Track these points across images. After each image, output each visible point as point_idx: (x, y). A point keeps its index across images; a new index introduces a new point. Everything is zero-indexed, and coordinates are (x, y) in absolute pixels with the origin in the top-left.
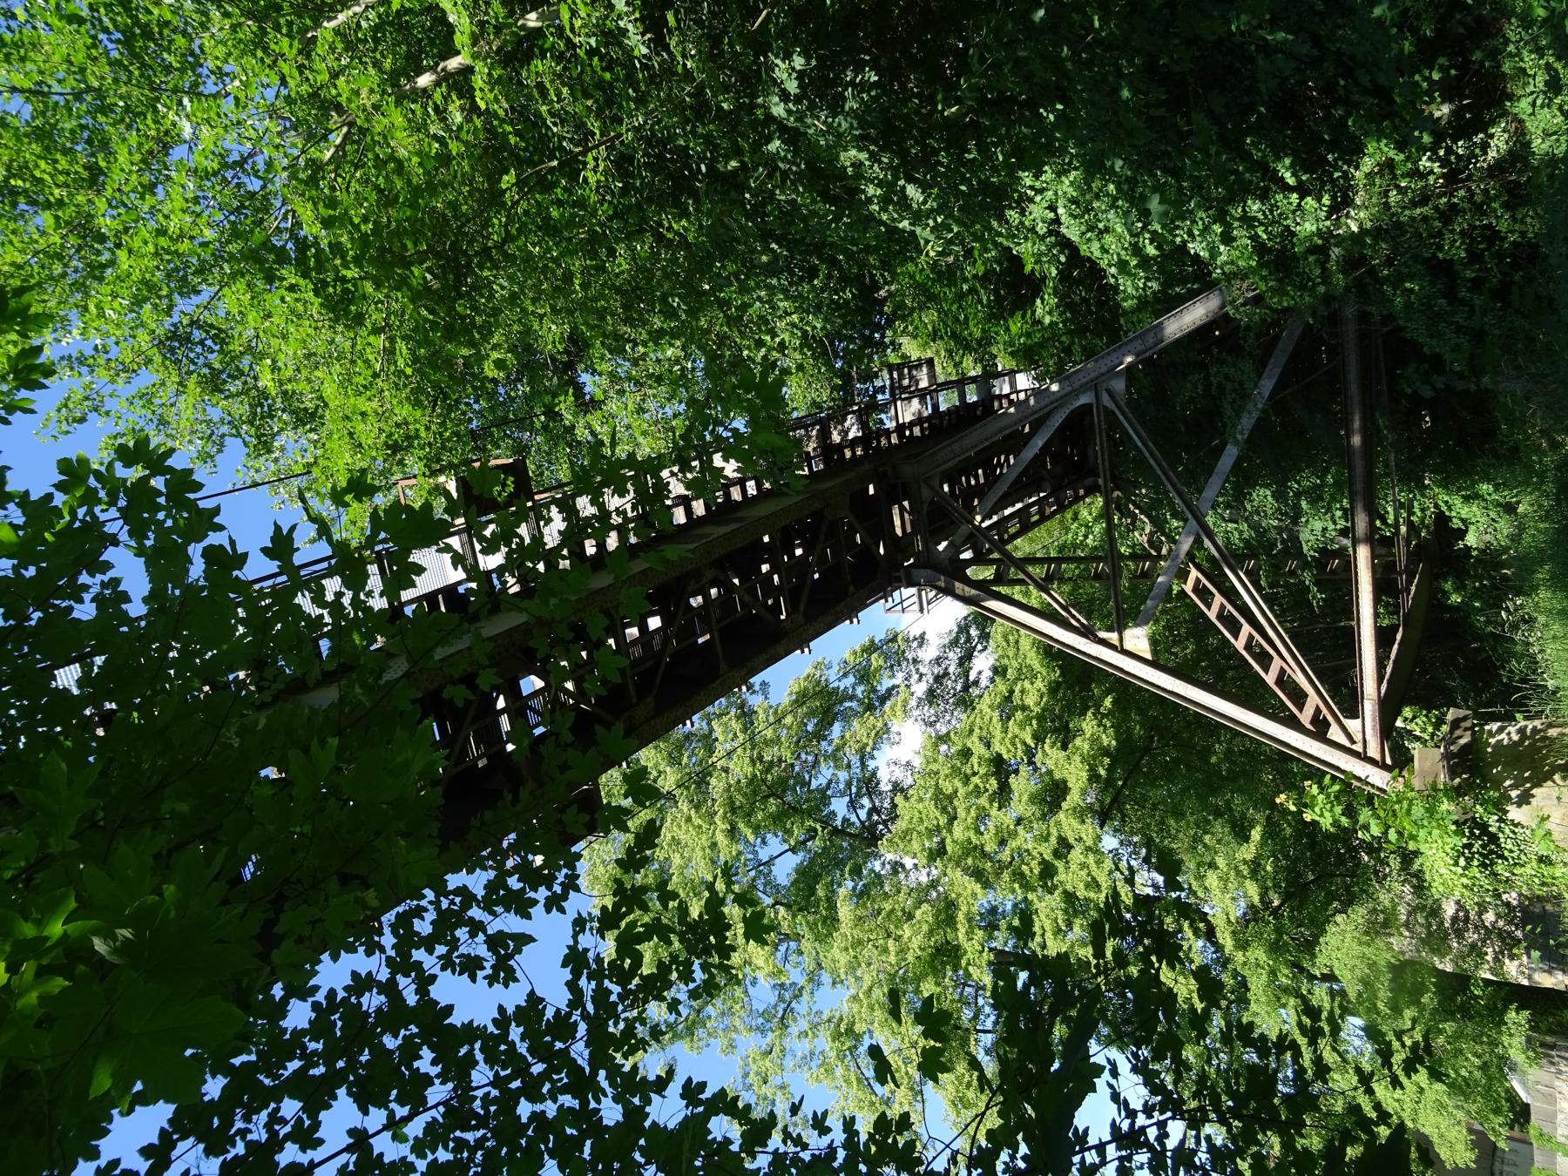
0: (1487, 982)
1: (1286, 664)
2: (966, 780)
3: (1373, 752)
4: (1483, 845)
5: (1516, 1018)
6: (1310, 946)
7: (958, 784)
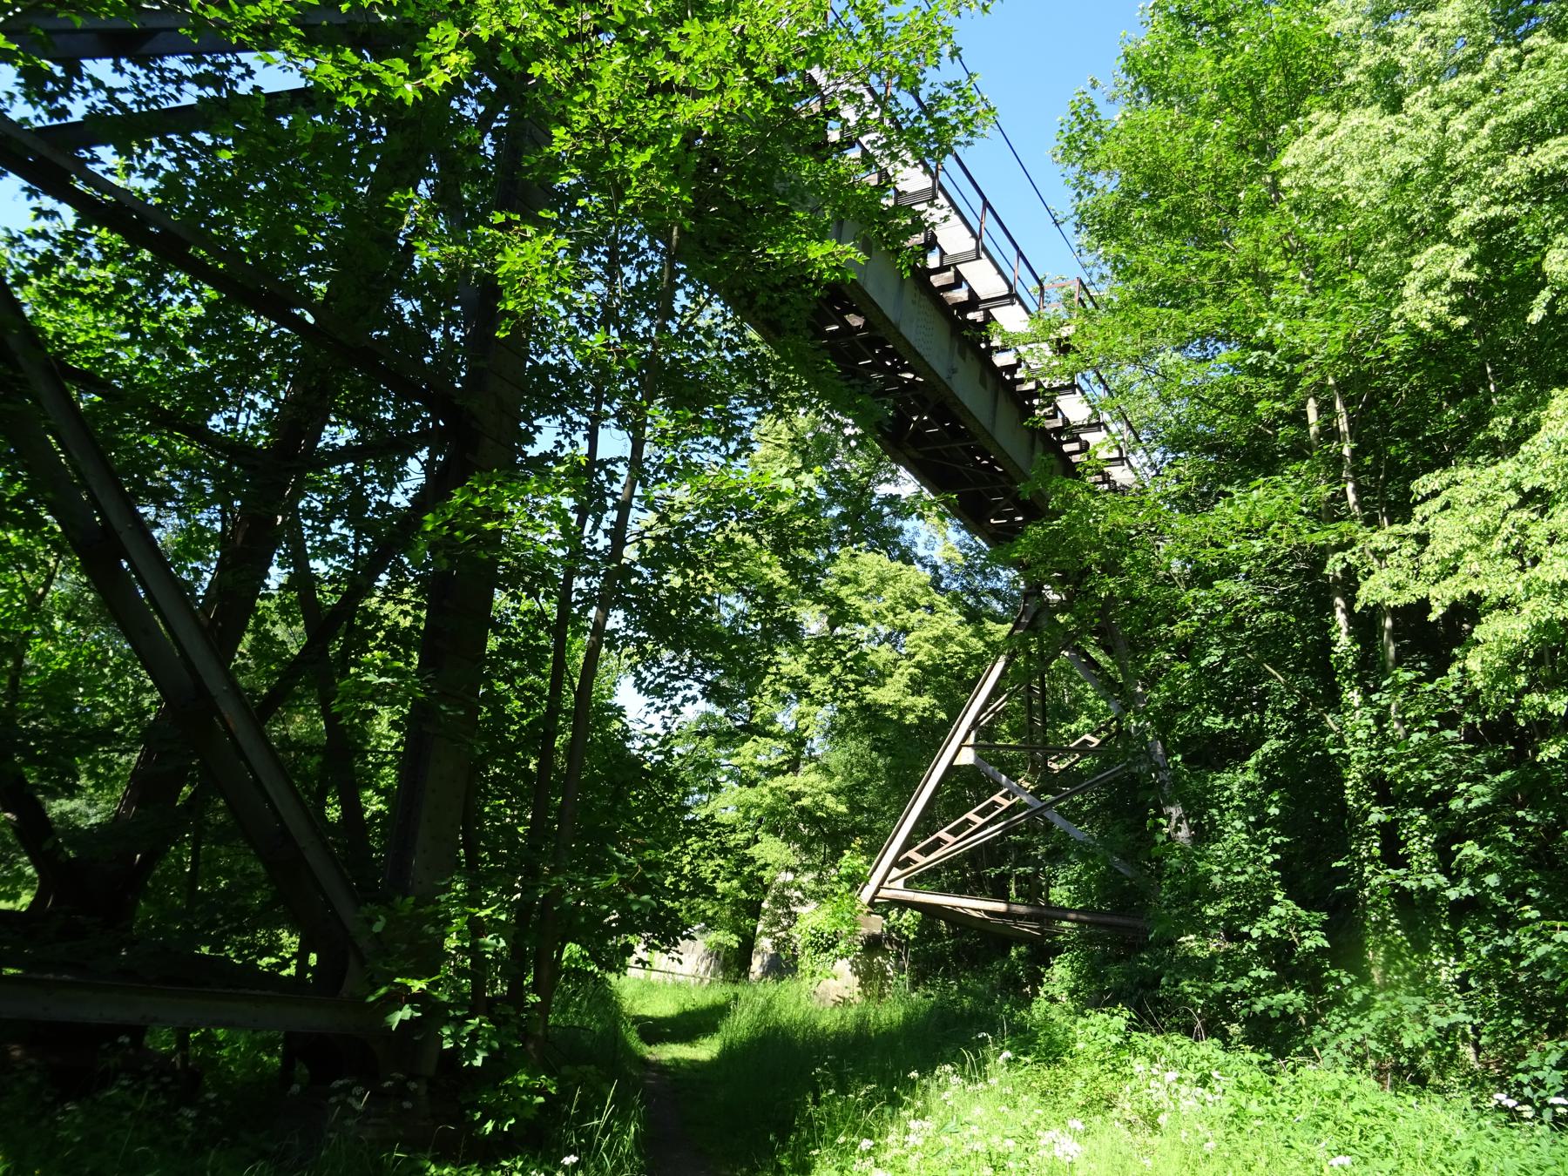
0: (755, 929)
1: (950, 844)
2: (892, 609)
3: (883, 893)
4: (825, 944)
5: (733, 941)
6: (774, 831)
7: (889, 602)
